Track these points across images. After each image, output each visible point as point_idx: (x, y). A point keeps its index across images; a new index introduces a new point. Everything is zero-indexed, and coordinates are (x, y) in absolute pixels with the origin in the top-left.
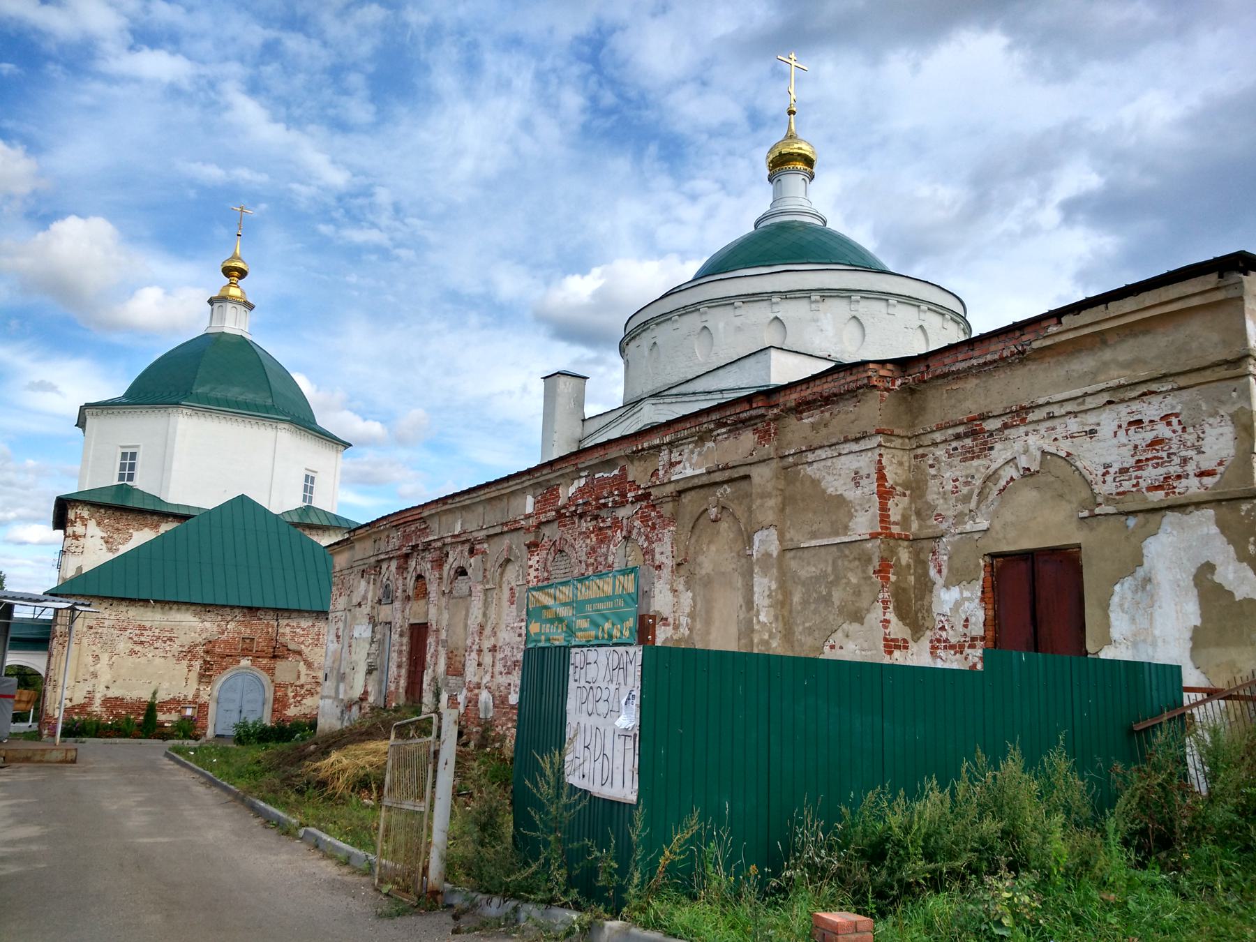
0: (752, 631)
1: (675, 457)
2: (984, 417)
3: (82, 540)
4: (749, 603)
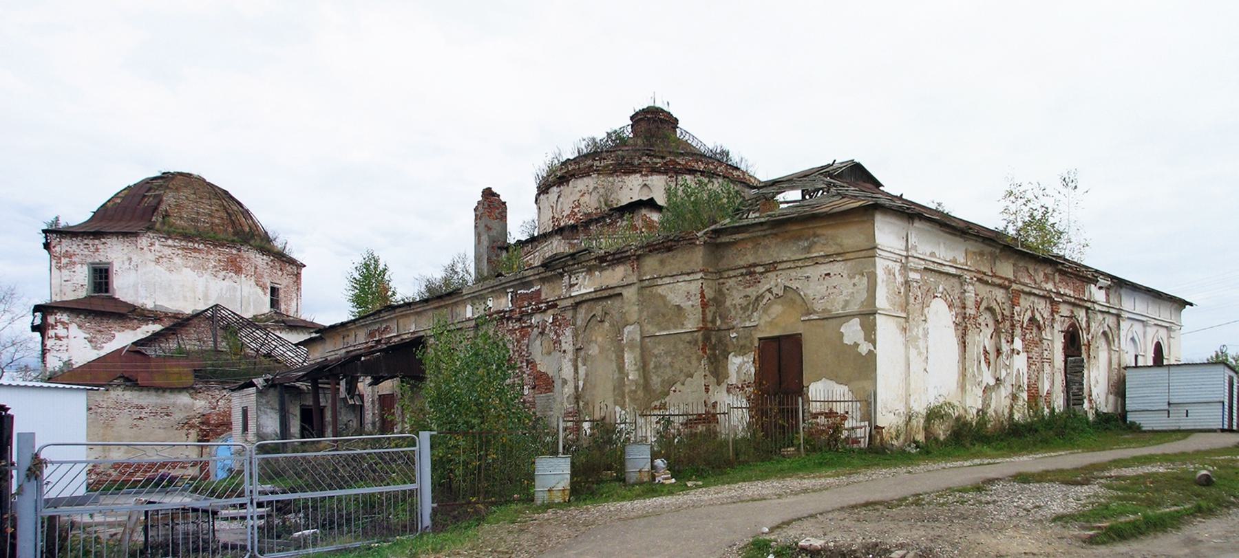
0: (624, 385)
1: (573, 281)
2: (755, 265)
3: (65, 341)
4: (621, 368)
